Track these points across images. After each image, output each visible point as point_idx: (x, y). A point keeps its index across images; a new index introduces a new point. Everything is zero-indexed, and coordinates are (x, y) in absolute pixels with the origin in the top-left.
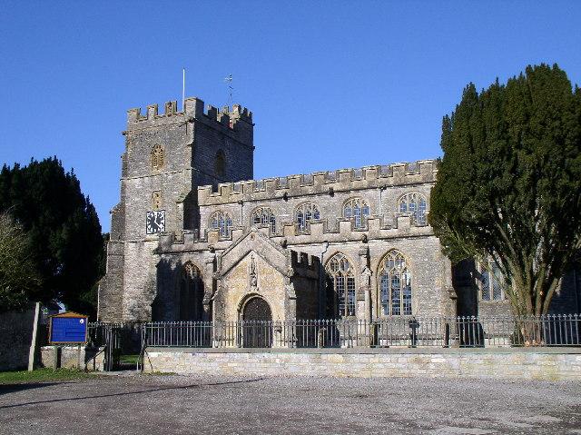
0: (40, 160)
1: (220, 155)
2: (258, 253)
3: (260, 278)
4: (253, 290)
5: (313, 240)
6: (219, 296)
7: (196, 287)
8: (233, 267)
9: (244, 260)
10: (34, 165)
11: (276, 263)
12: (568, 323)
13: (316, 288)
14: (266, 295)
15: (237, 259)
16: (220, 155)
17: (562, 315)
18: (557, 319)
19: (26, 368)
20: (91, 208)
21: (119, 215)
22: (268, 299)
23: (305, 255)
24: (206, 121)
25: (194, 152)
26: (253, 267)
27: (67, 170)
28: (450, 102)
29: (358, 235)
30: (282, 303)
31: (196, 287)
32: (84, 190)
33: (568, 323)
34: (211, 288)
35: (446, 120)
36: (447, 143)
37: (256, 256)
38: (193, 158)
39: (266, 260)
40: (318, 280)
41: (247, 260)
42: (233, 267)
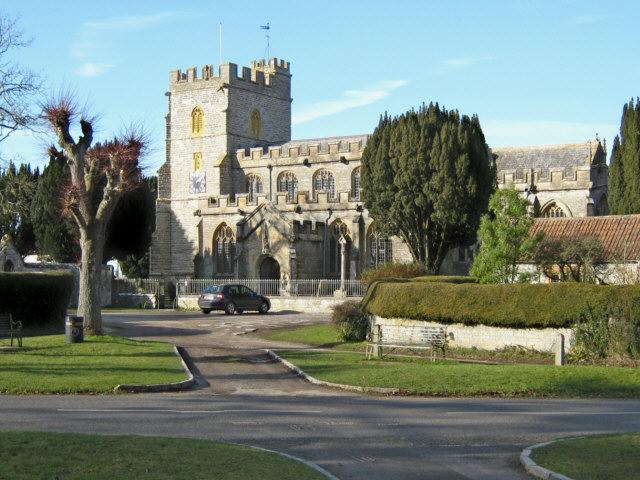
24: (241, 84)
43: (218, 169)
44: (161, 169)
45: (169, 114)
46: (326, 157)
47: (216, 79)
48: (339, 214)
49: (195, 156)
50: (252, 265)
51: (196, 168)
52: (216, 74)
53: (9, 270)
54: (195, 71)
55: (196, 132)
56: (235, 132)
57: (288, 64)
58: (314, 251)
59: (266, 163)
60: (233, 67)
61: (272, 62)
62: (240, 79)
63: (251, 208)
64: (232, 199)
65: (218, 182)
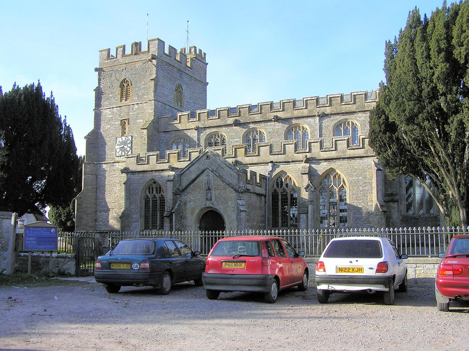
0: (22, 86)
1: (179, 89)
2: (212, 171)
3: (214, 193)
4: (209, 204)
5: (261, 161)
6: (177, 210)
7: (158, 202)
8: (190, 184)
9: (201, 178)
10: (16, 91)
11: (229, 179)
12: (399, 236)
13: (263, 203)
14: (220, 208)
15: (193, 176)
16: (179, 89)
17: (219, 231)
18: (432, 231)
19: (27, 272)
20: (68, 128)
21: (95, 140)
22: (222, 212)
23: (253, 174)
24: (167, 59)
25: (156, 85)
26: (208, 183)
27: (47, 95)
28: (395, 26)
29: (301, 157)
30: (234, 216)
31: (158, 202)
32: (62, 113)
33: (399, 236)
34: (171, 202)
35: (388, 45)
36: (390, 68)
37: (211, 174)
38: (155, 92)
39: (220, 177)
40: (265, 196)
41: (203, 177)
42: (190, 184)
43: (145, 131)
44: (89, 135)
45: (100, 279)
46: (258, 118)
47: (144, 53)
48: (282, 167)
49: (123, 123)
50: (192, 219)
51: (124, 133)
52: (144, 48)
53: (385, 271)
54: (124, 47)
55: (123, 101)
56: (160, 99)
57: (205, 54)
58: (258, 204)
59: (193, 126)
60: (161, 43)
61: (193, 50)
62: (166, 54)
63: (182, 165)
64: (161, 157)
65: (146, 142)
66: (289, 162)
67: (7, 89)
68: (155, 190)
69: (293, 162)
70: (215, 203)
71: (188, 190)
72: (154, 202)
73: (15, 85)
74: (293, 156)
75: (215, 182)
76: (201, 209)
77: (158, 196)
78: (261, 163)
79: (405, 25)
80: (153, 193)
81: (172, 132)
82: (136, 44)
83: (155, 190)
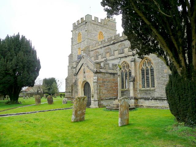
5: (116, 57)
10: (8, 38)
66: (127, 57)
67: (3, 38)
68: (126, 67)
69: (128, 56)
70: (87, 79)
71: (79, 73)
72: (147, 70)
73: (8, 35)
74: (128, 53)
75: (87, 70)
76: (83, 82)
77: (127, 70)
78: (116, 59)
79: (5, 38)
80: (146, 65)
81: (108, 44)
82: (81, 18)
83: (126, 67)
